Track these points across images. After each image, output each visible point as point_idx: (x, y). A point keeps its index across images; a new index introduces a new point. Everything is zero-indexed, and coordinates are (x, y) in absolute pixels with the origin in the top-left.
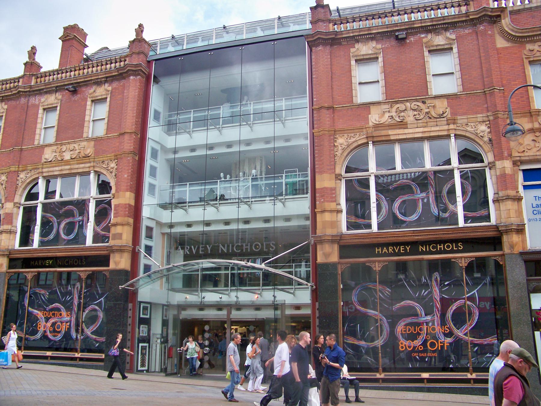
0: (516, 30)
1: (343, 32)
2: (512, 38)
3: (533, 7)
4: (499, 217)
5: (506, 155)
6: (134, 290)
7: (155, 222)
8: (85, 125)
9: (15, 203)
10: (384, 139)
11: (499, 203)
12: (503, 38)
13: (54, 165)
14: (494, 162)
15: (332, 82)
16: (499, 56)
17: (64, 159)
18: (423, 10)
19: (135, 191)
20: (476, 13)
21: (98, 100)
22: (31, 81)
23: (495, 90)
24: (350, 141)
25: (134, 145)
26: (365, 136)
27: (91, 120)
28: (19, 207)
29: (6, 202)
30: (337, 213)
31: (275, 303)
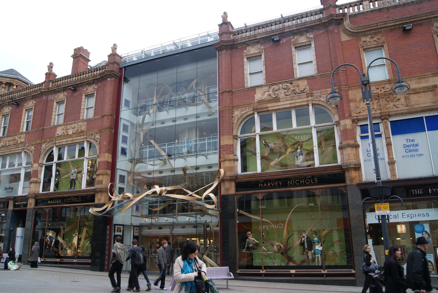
0: (353, 28)
1: (238, 40)
2: (351, 34)
3: (365, 12)
4: (343, 159)
5: (347, 116)
6: (110, 217)
7: (126, 172)
8: (81, 112)
9: (39, 164)
10: (264, 110)
11: (343, 149)
12: (346, 34)
13: (63, 138)
14: (339, 121)
15: (231, 74)
16: (342, 47)
17: (69, 134)
18: (292, 19)
19: (112, 153)
20: (326, 18)
21: (89, 95)
22: (49, 85)
23: (340, 71)
24: (242, 113)
25: (110, 123)
26: (252, 109)
27: (85, 108)
28: (42, 167)
29: (34, 163)
30: (234, 161)
31: (197, 222)
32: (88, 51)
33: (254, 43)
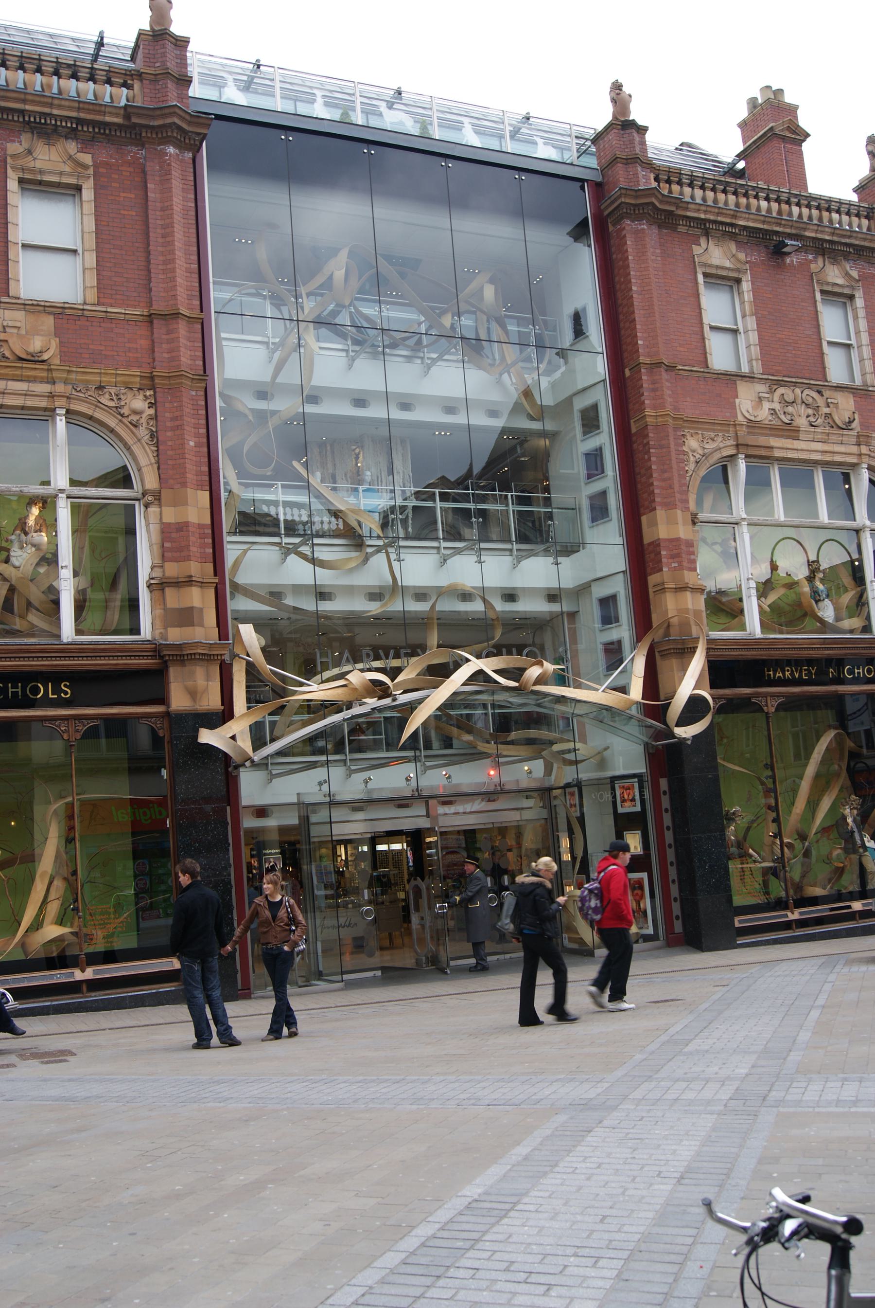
21: (40, 183)
32: (743, 113)
33: (723, 235)
